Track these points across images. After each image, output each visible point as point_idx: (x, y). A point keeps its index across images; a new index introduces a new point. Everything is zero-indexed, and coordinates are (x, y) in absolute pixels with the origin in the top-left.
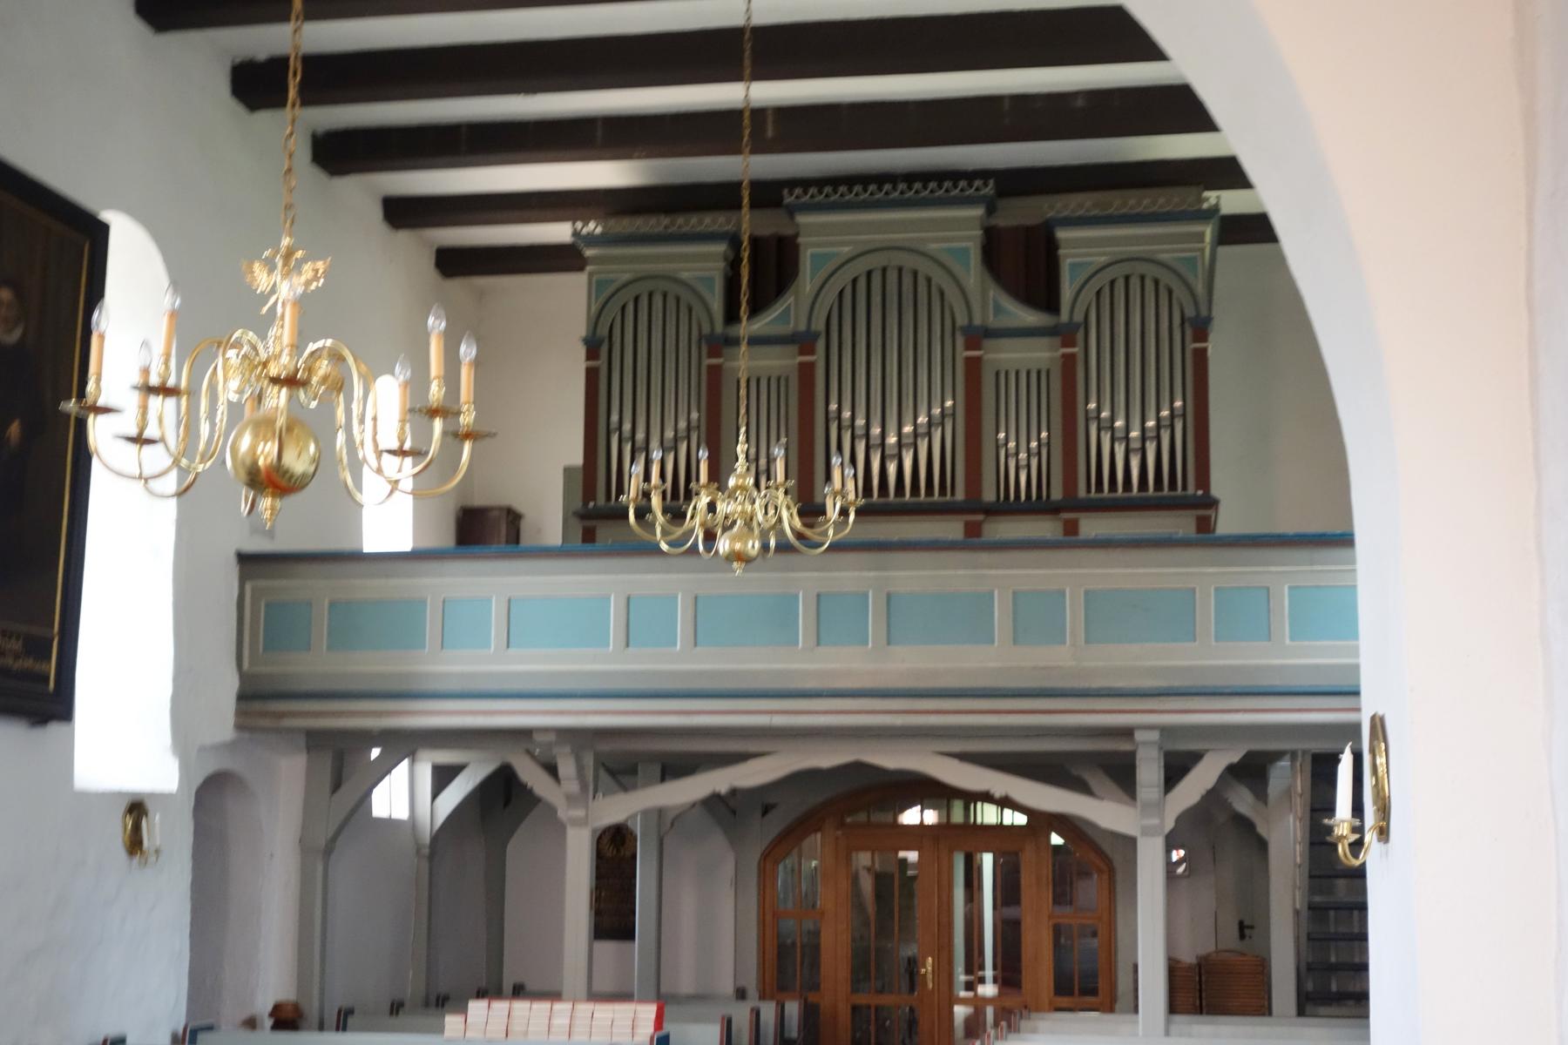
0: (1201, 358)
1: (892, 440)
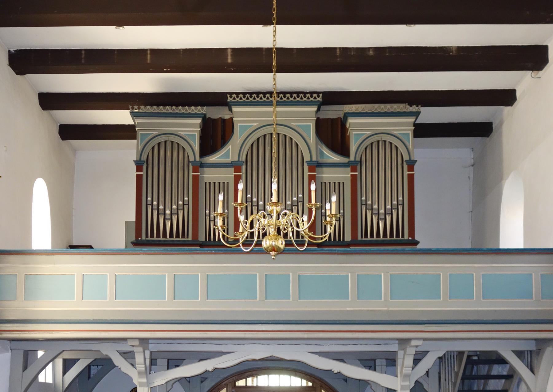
0: (411, 178)
1: (168, 212)
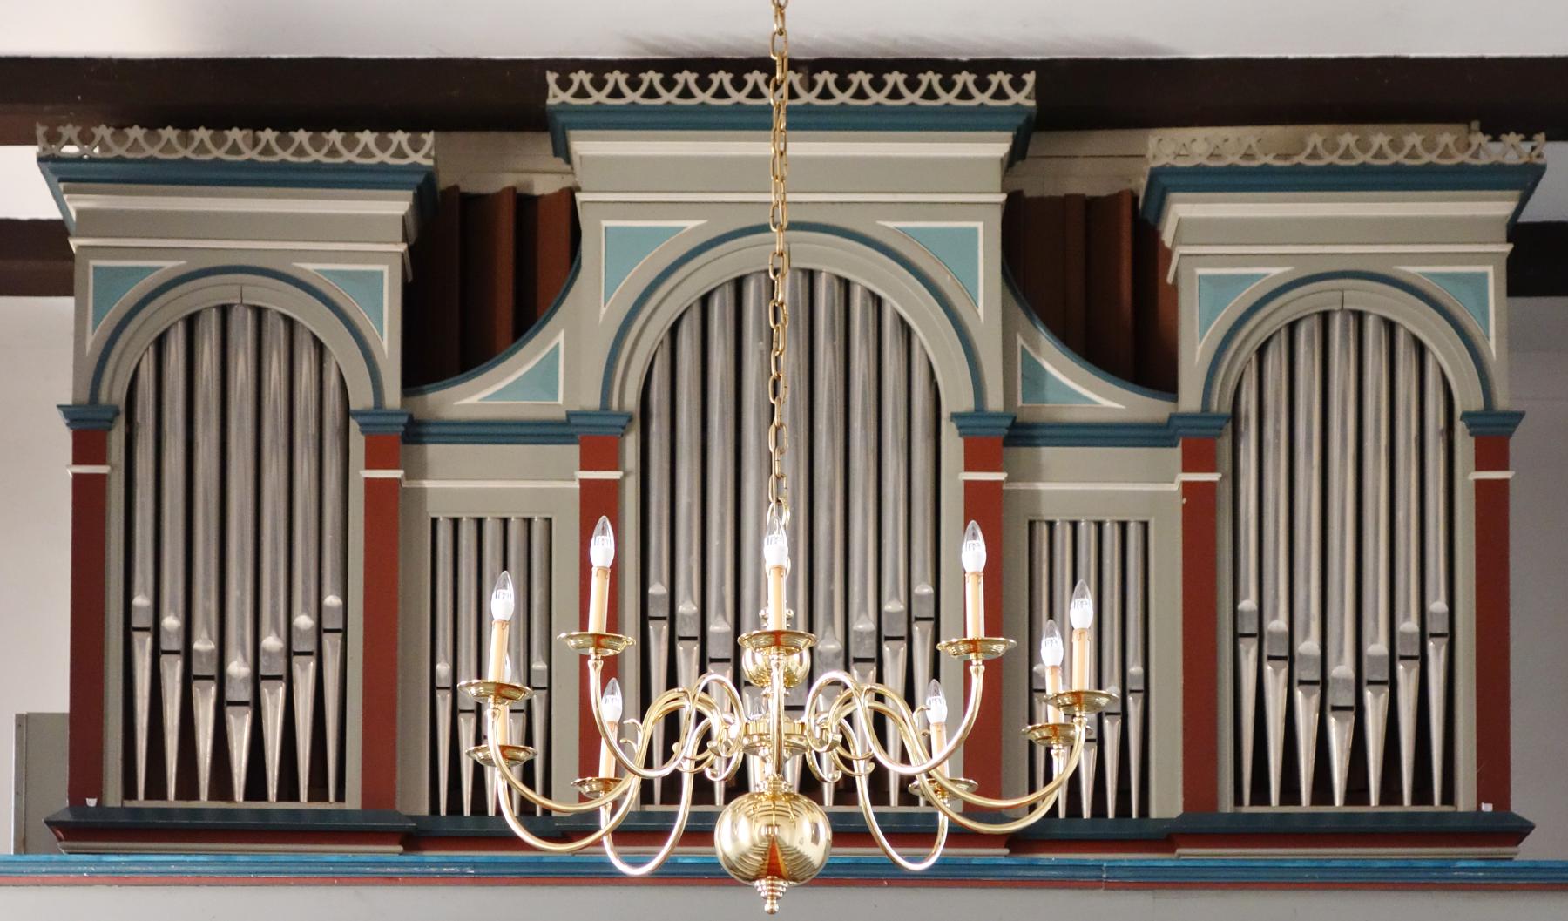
0: (1492, 500)
1: (238, 668)
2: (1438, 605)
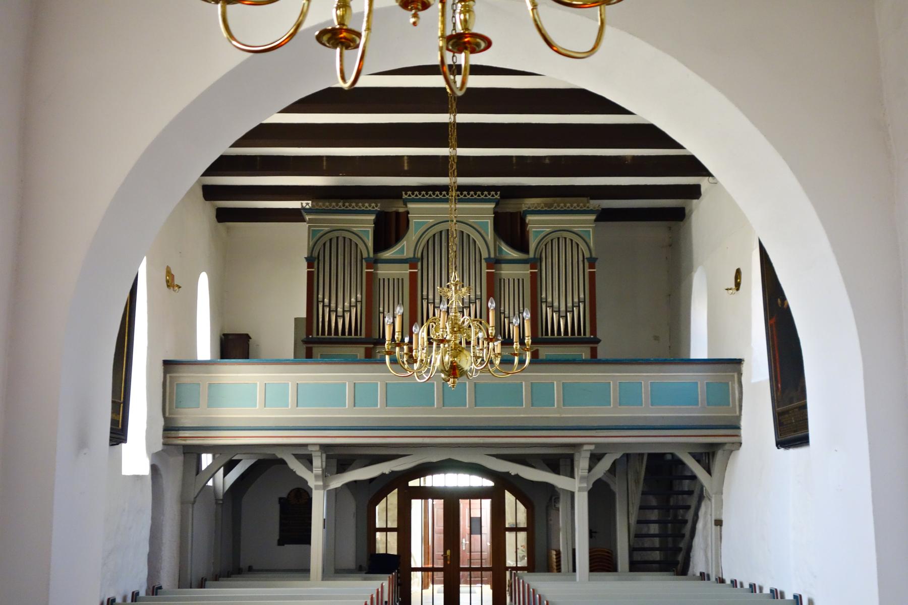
0: (592, 276)
1: (340, 310)
2: (582, 296)
